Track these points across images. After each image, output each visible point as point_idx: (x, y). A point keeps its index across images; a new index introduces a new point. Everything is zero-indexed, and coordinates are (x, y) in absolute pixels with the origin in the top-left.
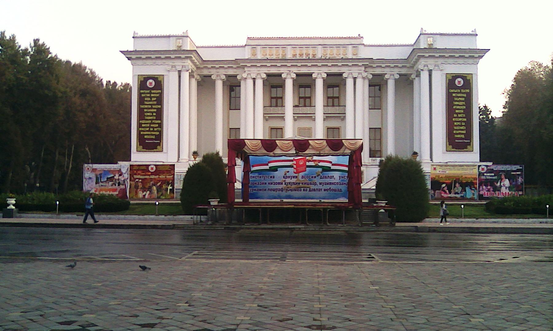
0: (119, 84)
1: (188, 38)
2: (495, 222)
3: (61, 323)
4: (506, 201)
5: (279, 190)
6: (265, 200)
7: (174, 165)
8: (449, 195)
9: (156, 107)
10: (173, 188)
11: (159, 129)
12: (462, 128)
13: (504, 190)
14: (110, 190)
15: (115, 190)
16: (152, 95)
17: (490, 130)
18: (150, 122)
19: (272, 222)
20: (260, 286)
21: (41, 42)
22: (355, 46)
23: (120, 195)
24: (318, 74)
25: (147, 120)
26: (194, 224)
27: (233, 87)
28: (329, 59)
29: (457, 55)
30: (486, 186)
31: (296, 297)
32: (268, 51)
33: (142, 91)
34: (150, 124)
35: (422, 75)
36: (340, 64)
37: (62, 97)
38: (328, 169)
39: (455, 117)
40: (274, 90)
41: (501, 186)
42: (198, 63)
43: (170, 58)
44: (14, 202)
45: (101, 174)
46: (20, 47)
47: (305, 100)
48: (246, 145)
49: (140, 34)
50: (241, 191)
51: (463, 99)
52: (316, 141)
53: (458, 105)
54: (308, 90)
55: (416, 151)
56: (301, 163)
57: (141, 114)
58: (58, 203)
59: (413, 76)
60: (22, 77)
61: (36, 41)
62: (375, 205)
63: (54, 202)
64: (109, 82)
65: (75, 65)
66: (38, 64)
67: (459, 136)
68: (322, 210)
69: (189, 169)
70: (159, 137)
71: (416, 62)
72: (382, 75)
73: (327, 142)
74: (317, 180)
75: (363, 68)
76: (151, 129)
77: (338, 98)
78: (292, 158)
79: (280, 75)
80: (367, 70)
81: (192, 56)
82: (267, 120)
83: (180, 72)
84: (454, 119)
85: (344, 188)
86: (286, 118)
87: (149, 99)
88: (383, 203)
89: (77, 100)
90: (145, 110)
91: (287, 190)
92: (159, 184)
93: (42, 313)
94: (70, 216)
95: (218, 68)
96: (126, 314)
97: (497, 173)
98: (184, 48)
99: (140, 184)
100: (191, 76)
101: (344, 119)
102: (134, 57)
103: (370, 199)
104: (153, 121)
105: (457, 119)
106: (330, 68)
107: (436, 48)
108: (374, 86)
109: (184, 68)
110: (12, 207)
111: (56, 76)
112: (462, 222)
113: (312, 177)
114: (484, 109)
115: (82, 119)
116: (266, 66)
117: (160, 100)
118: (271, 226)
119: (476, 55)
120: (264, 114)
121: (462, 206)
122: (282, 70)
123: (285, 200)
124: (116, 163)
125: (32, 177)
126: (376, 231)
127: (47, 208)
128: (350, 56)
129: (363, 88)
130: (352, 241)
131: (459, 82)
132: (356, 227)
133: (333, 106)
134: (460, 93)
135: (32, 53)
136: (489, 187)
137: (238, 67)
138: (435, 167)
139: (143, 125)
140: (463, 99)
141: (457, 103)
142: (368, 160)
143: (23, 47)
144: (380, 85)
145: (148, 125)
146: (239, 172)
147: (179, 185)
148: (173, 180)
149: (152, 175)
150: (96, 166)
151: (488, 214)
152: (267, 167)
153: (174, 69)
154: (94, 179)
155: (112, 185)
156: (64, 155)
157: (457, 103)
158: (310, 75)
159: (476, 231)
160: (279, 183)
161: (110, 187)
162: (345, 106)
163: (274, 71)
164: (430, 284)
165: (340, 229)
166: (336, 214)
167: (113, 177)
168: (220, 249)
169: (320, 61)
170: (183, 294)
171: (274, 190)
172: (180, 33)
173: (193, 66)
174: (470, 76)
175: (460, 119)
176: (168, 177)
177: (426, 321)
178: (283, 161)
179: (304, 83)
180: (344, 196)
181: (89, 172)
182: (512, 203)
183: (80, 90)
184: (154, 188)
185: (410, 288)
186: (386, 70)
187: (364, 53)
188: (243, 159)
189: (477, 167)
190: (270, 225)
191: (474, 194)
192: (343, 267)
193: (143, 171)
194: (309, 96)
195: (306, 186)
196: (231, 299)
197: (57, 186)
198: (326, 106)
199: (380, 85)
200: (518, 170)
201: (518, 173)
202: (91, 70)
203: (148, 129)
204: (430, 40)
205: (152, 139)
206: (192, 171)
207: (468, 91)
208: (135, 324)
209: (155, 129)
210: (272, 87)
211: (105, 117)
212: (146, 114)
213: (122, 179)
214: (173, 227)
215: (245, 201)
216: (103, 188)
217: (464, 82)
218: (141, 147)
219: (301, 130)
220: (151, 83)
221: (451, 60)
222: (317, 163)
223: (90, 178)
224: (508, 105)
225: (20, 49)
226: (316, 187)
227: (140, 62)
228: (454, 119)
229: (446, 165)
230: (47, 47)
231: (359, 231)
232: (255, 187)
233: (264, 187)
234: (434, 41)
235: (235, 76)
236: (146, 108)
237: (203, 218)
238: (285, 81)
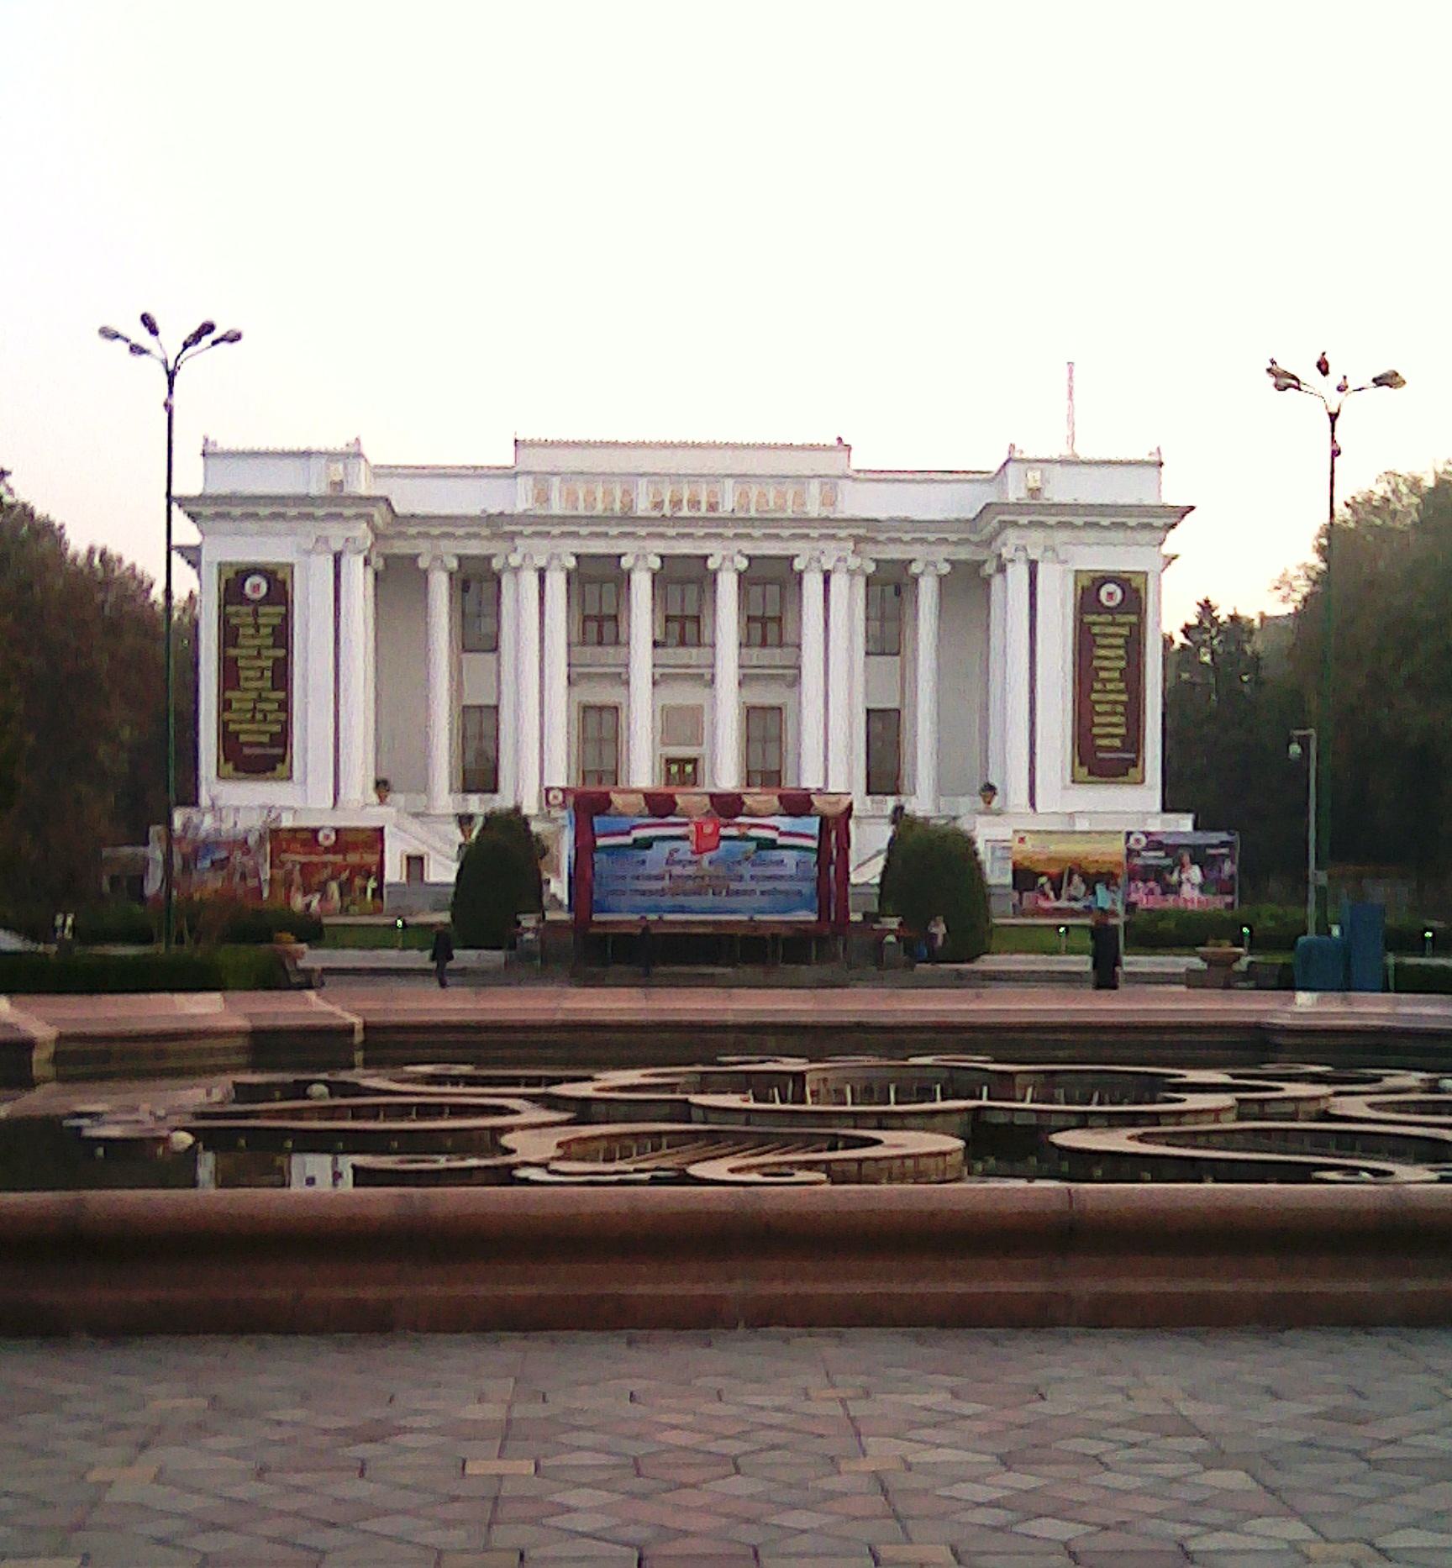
6: (621, 917)
8: (1057, 904)
9: (271, 653)
12: (1115, 719)
13: (1187, 891)
22: (830, 482)
25: (246, 690)
27: (478, 587)
30: (1145, 881)
38: (772, 845)
41: (1180, 883)
47: (683, 626)
49: (225, 443)
51: (1120, 641)
53: (1106, 658)
55: (996, 784)
57: (229, 675)
59: (990, 568)
70: (283, 739)
74: (746, 870)
75: (851, 545)
80: (862, 546)
85: (808, 888)
88: (893, 923)
92: (345, 875)
98: (348, 489)
101: (795, 681)
117: (283, 635)
129: (849, 598)
131: (1110, 595)
134: (1113, 624)
136: (1152, 884)
140: (1120, 641)
141: (1102, 652)
152: (628, 840)
153: (321, 547)
157: (1102, 652)
171: (643, 893)
172: (337, 444)
175: (1112, 697)
179: (684, 582)
184: (334, 887)
187: (858, 503)
189: (1123, 837)
193: (304, 843)
200: (1223, 844)
204: (1034, 477)
205: (261, 744)
220: (256, 587)
221: (1091, 535)
222: (744, 830)
234: (1045, 480)
235: (488, 559)
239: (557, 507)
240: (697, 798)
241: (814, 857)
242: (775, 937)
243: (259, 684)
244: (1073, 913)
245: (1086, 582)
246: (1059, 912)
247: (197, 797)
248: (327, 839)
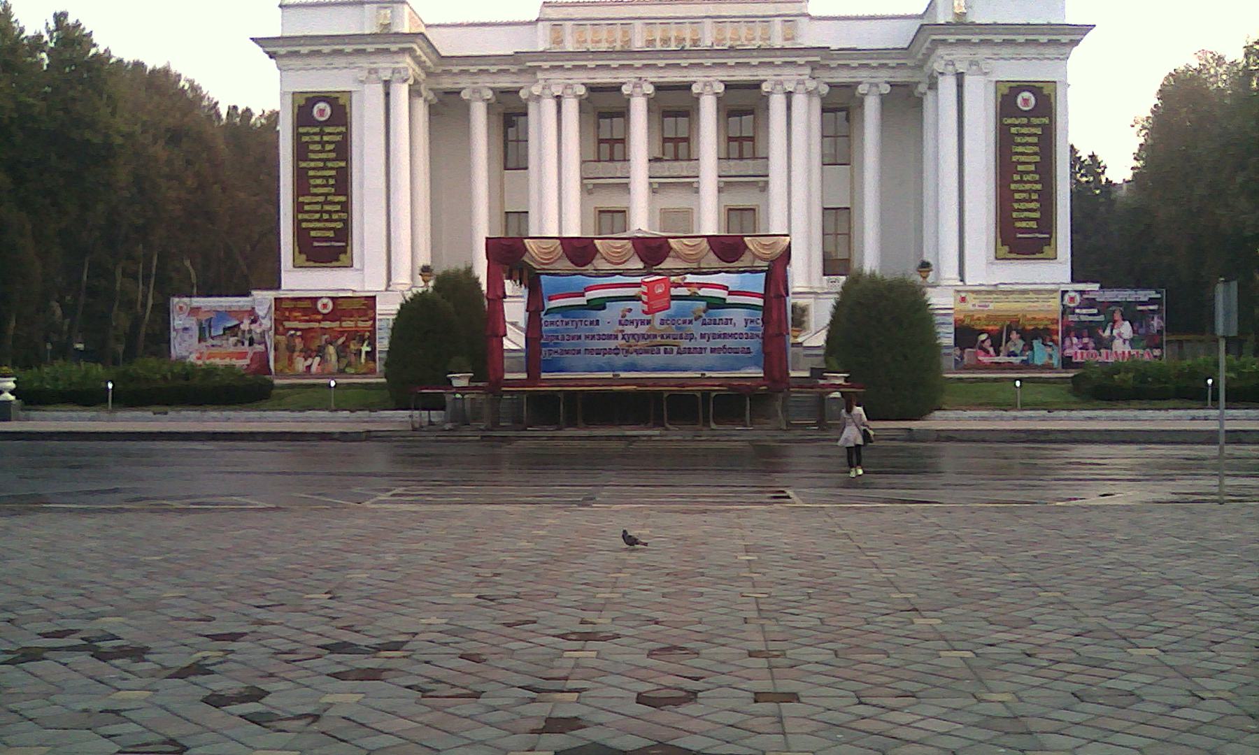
0: (257, 112)
1: (406, 7)
2: (1090, 418)
3: (46, 635)
5: (610, 351)
6: (580, 374)
7: (374, 297)
8: (997, 359)
10: (374, 349)
11: (344, 215)
13: (1119, 346)
14: (231, 355)
15: (242, 355)
16: (326, 138)
17: (1102, 209)
18: (321, 199)
19: (589, 422)
20: (502, 557)
21: (71, 20)
22: (789, 20)
23: (254, 366)
24: (705, 85)
26: (414, 430)
27: (510, 117)
28: (731, 48)
29: (1021, 39)
31: (570, 579)
33: (302, 130)
34: (322, 204)
35: (940, 86)
36: (755, 62)
37: (121, 146)
38: (719, 304)
41: (1112, 338)
42: (429, 63)
45: (209, 320)
46: (22, 30)
47: (675, 146)
48: (526, 250)
50: (523, 354)
51: (1035, 140)
53: (1022, 154)
54: (683, 121)
55: (930, 260)
57: (301, 179)
58: (110, 386)
59: (922, 88)
60: (31, 100)
61: (60, 18)
62: (821, 382)
63: (103, 385)
64: (235, 108)
67: (1024, 224)
68: (699, 395)
69: (402, 305)
70: (344, 234)
71: (927, 56)
72: (851, 87)
74: (696, 328)
75: (807, 71)
76: (326, 216)
78: (638, 280)
79: (617, 88)
80: (817, 73)
81: (415, 46)
82: (590, 192)
83: (387, 83)
84: (1013, 186)
85: (755, 345)
87: (318, 147)
89: (159, 151)
90: (311, 173)
91: (627, 352)
93: (12, 616)
96: (189, 615)
97: (1104, 307)
99: (298, 341)
100: (414, 92)
101: (765, 188)
103: (812, 370)
104: (329, 198)
105: (1020, 187)
107: (973, 24)
108: (834, 110)
111: (109, 97)
112: (1015, 418)
113: (684, 322)
114: (1089, 162)
117: (343, 150)
119: (1065, 39)
120: (582, 178)
121: (1018, 383)
123: (623, 375)
124: (247, 294)
125: (66, 328)
126: (819, 440)
127: (87, 398)
128: (778, 43)
129: (806, 114)
130: (765, 463)
131: (1026, 101)
132: (775, 433)
133: (741, 158)
135: (52, 45)
136: (1086, 340)
137: (521, 71)
138: (963, 295)
139: (307, 208)
140: (1035, 140)
141: (1020, 149)
142: (821, 280)
143: (29, 32)
144: (846, 110)
145: (318, 207)
146: (515, 310)
147: (383, 344)
148: (373, 332)
149: (324, 320)
150: (198, 301)
151: (1074, 399)
153: (374, 76)
154: (193, 331)
155: (235, 345)
157: (1020, 149)
158: (687, 87)
159: (1043, 438)
160: (609, 337)
161: (232, 349)
162: (767, 158)
163: (604, 78)
164: (872, 549)
165: (739, 436)
166: (731, 404)
167: (237, 326)
168: (454, 483)
169: (708, 54)
170: (329, 576)
173: (418, 70)
174: (1051, 86)
175: (1028, 186)
176: (360, 324)
177: (818, 622)
178: (617, 284)
179: (674, 106)
180: (757, 365)
182: (1131, 375)
183: (168, 130)
184: (331, 349)
186: (862, 75)
187: (811, 36)
188: (526, 280)
189: (1059, 294)
191: (1051, 356)
193: (305, 311)
194: (686, 135)
195: (670, 341)
196: (424, 585)
197: (120, 348)
198: (724, 158)
199: (846, 110)
200: (1152, 301)
201: (1151, 307)
202: (191, 82)
203: (317, 216)
206: (413, 310)
207: (1046, 120)
208: (200, 635)
209: (335, 216)
211: (224, 190)
212: (312, 182)
213: (258, 331)
214: (368, 436)
215: (533, 377)
216: (214, 350)
218: (1007, 248)
219: (732, 212)
220: (322, 111)
221: (1006, 51)
223: (186, 329)
224: (1145, 152)
226: (692, 344)
228: (1013, 186)
229: (994, 291)
230: (87, 31)
236: (314, 169)
237: (436, 416)
238: (698, 99)
239: (570, 46)
240: (619, 243)
241: (760, 314)
242: (706, 394)
243: (325, 190)
244: (1011, 367)
246: (999, 367)
247: (1212, 431)
248: (325, 307)
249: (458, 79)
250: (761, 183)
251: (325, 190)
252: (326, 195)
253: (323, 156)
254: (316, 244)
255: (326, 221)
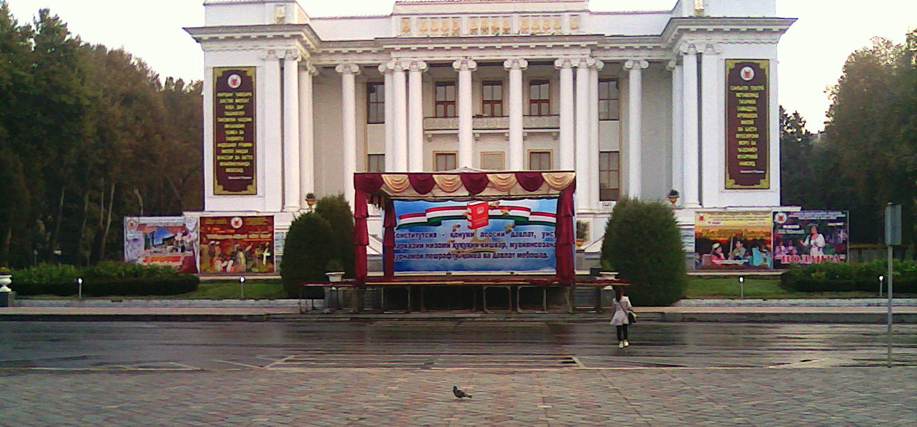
0: (187, 82)
1: (295, 5)
2: (794, 305)
4: (814, 271)
5: (444, 256)
6: (422, 273)
8: (726, 262)
10: (272, 254)
11: (250, 157)
12: (752, 150)
13: (815, 252)
14: (168, 259)
15: (176, 259)
16: (237, 101)
17: (803, 152)
18: (234, 145)
20: (365, 406)
21: (51, 15)
22: (574, 14)
23: (185, 267)
24: (514, 62)
26: (302, 313)
27: (372, 85)
28: (533, 35)
29: (744, 28)
30: (786, 245)
31: (415, 422)
32: (429, 24)
34: (235, 148)
35: (685, 63)
37: (89, 106)
38: (525, 222)
39: (740, 133)
40: (441, 89)
41: (810, 247)
42: (312, 46)
43: (264, 38)
44: (9, 281)
45: (153, 233)
46: (16, 23)
47: (492, 106)
48: (383, 182)
50: (381, 258)
51: (754, 102)
52: (499, 175)
54: (497, 88)
55: (678, 191)
56: (481, 212)
57: (220, 134)
58: (80, 281)
59: (672, 64)
60: (23, 73)
61: (43, 13)
62: (598, 278)
63: (75, 280)
64: (171, 78)
65: (112, 51)
66: (49, 51)
67: (746, 164)
68: (509, 288)
69: (293, 223)
70: (251, 171)
71: (675, 41)
72: (620, 63)
73: (516, 177)
74: (507, 239)
75: (588, 51)
76: (237, 158)
77: (547, 101)
78: (465, 204)
79: (449, 64)
81: (302, 34)
82: (430, 140)
83: (282, 61)
84: (738, 136)
85: (550, 251)
86: (460, 136)
87: (232, 107)
89: (116, 110)
90: (227, 126)
92: (248, 248)
94: (101, 301)
95: (345, 54)
97: (804, 224)
99: (217, 248)
100: (301, 67)
101: (557, 137)
102: (205, 37)
103: (592, 270)
104: (240, 144)
105: (743, 136)
106: (431, 54)
107: (708, 17)
108: (608, 80)
109: (289, 55)
110: (6, 289)
111: (80, 71)
112: (739, 305)
113: (499, 235)
114: (793, 118)
115: (125, 142)
116: (460, 48)
117: (250, 109)
118: (427, 315)
119: (775, 28)
120: (424, 130)
121: (741, 279)
122: (453, 56)
123: (454, 273)
124: (180, 215)
125: (48, 239)
127: (63, 290)
129: (588, 83)
130: (558, 337)
131: (747, 74)
132: (564, 316)
133: (540, 115)
135: (38, 33)
136: (791, 248)
137: (379, 52)
138: (702, 215)
139: (223, 151)
140: (754, 102)
141: (743, 109)
143: (21, 24)
144: (616, 80)
145: (231, 151)
146: (375, 226)
148: (272, 242)
149: (236, 233)
150: (144, 220)
153: (272, 55)
154: (141, 242)
155: (171, 251)
156: (98, 201)
157: (743, 109)
158: (501, 63)
159: (759, 319)
160: (444, 246)
161: (169, 255)
162: (559, 115)
163: (440, 57)
164: (635, 400)
165: (539, 318)
166: (532, 294)
167: (173, 238)
168: (331, 352)
169: (516, 40)
173: (304, 51)
175: (748, 136)
176: (262, 236)
178: (449, 208)
179: (491, 77)
180: (551, 266)
181: (133, 231)
182: (823, 273)
183: (122, 95)
185: (599, 407)
186: (628, 55)
187: (590, 26)
189: (771, 214)
190: (427, 312)
191: (765, 260)
192: (515, 377)
193: (222, 227)
195: (488, 248)
197: (88, 254)
198: (527, 115)
199: (616, 80)
200: (839, 220)
201: (839, 224)
203: (231, 157)
206: (301, 226)
207: (762, 88)
209: (244, 158)
210: (438, 84)
211: (163, 138)
212: (227, 132)
213: (188, 241)
214: (268, 318)
215: (388, 275)
216: (156, 255)
217: (740, 71)
221: (733, 37)
223: (135, 240)
224: (836, 111)
225: (17, 26)
226: (504, 251)
227: (215, 46)
228: (738, 136)
229: (724, 212)
231: (570, 321)
232: (405, 251)
233: (419, 251)
236: (228, 123)
237: (317, 303)
238: (508, 72)
240: (450, 177)
242: (514, 287)
243: (237, 139)
244: (736, 267)
245: (732, 65)
247: (883, 314)
248: (237, 223)
249: (333, 58)
250: (554, 134)
251: (237, 139)
252: (237, 142)
253: (235, 113)
254: (230, 178)
255: (238, 161)
